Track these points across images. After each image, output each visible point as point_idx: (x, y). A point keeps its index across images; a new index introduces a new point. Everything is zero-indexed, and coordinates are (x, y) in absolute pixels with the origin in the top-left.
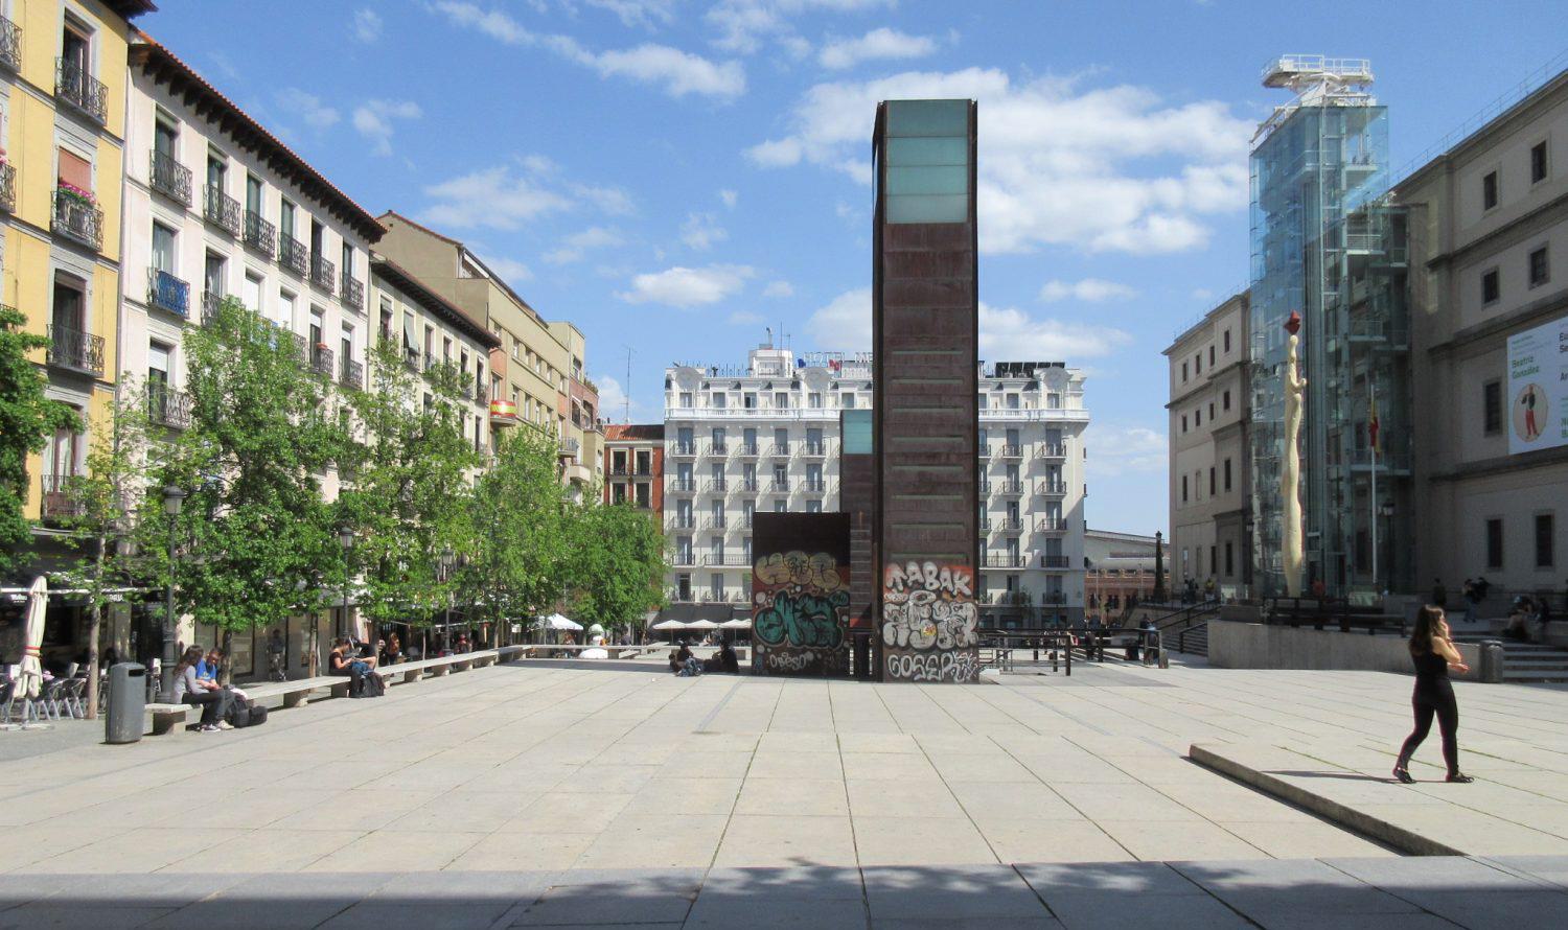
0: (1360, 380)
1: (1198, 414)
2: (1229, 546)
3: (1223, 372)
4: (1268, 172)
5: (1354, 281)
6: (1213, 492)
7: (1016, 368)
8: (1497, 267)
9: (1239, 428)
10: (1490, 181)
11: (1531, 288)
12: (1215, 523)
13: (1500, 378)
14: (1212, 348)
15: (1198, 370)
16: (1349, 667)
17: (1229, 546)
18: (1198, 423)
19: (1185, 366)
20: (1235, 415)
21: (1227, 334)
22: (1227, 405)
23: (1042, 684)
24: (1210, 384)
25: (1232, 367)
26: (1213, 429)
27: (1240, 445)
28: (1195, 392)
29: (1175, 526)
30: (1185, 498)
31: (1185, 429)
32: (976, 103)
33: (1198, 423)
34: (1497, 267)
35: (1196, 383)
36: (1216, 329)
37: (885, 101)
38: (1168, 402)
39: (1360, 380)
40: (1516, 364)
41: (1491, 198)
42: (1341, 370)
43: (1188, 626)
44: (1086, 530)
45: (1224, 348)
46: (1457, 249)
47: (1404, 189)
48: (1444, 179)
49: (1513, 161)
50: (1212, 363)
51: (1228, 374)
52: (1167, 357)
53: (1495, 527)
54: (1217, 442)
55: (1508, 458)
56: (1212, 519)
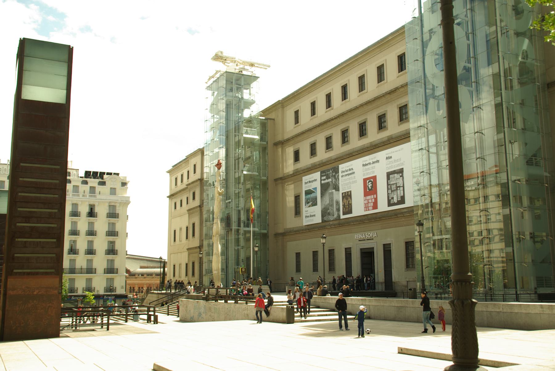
0: (248, 190)
1: (181, 201)
2: (193, 263)
3: (193, 183)
4: (213, 97)
5: (247, 148)
6: (187, 238)
7: (95, 175)
8: (299, 148)
9: (199, 208)
10: (297, 113)
11: (311, 158)
12: (187, 252)
13: (300, 193)
14: (188, 172)
15: (182, 182)
16: (226, 319)
17: (193, 263)
18: (181, 206)
19: (176, 179)
20: (197, 203)
21: (195, 166)
22: (194, 198)
23: (93, 335)
24: (187, 188)
25: (196, 181)
26: (188, 209)
27: (199, 217)
28: (180, 191)
29: (170, 254)
30: (175, 241)
31: (175, 208)
32: (73, 47)
33: (181, 206)
34: (299, 148)
35: (180, 186)
36: (190, 163)
37: (24, 38)
38: (168, 195)
39: (248, 190)
40: (343, 172)
41: (297, 121)
42: (241, 186)
43: (172, 302)
44: (127, 255)
45: (193, 172)
46: (285, 139)
47: (265, 112)
48: (280, 110)
49: (304, 107)
50: (188, 178)
51: (195, 184)
52: (169, 174)
53: (298, 255)
54: (189, 214)
55: (302, 227)
56: (186, 250)
